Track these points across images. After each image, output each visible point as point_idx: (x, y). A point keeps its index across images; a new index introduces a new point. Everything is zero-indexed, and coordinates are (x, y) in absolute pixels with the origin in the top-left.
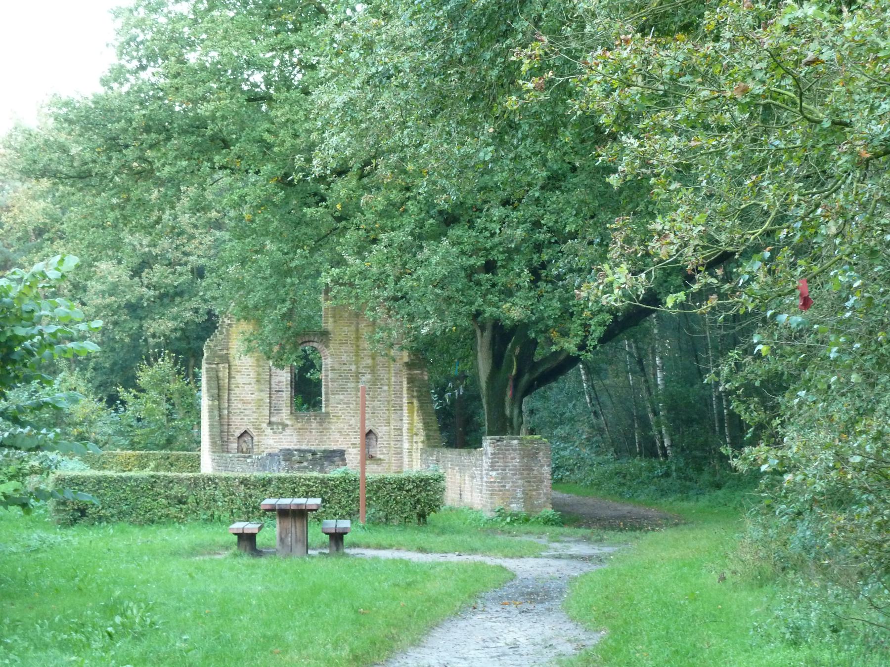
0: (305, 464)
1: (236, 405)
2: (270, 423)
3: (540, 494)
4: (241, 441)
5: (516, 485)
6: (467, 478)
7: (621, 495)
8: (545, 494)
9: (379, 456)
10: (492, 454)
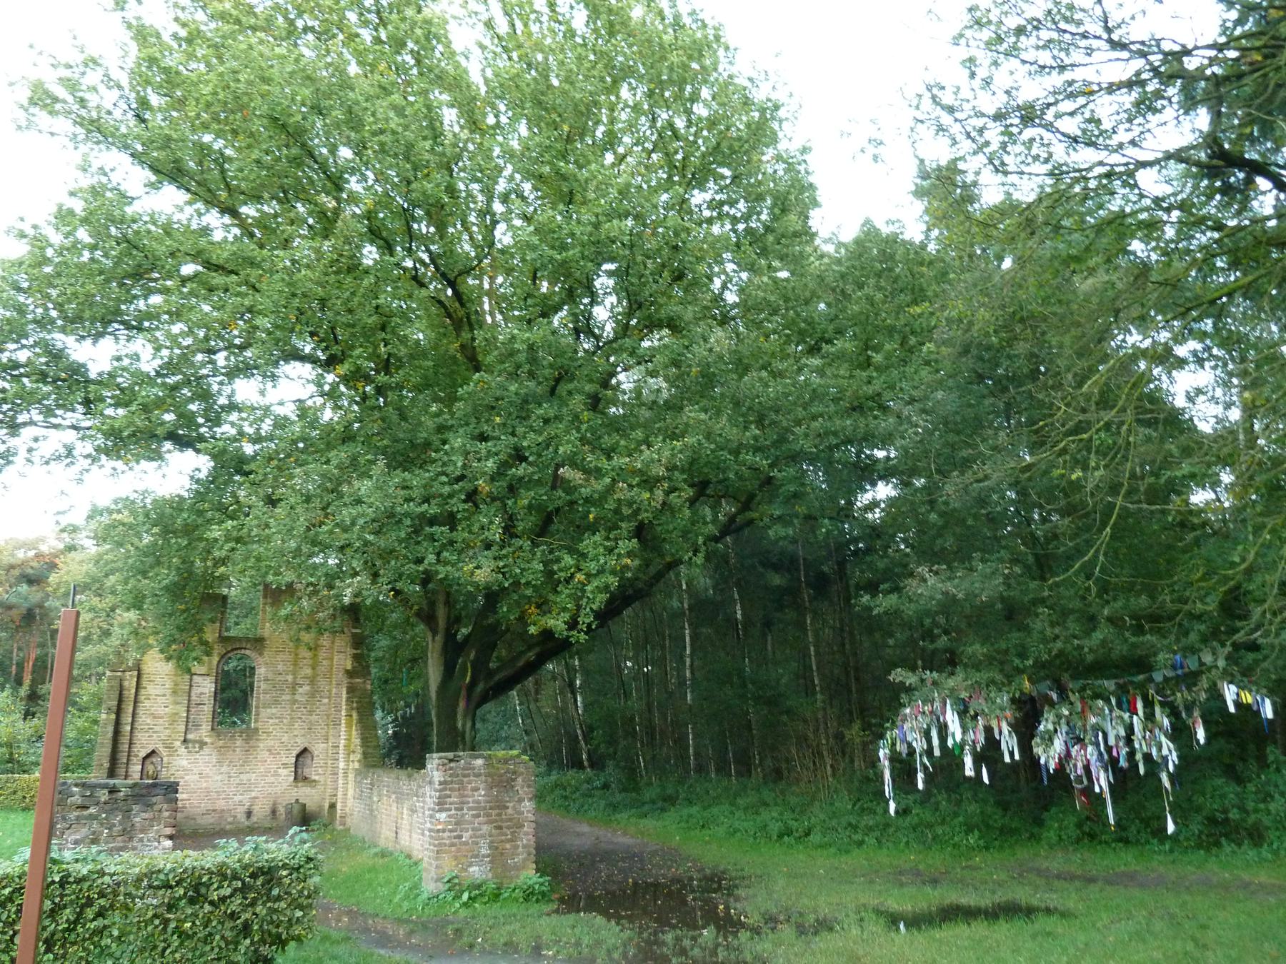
0: (93, 810)
1: (144, 719)
2: (185, 741)
3: (517, 847)
4: (148, 762)
5: (479, 833)
6: (405, 811)
7: (567, 808)
8: (524, 847)
9: (314, 777)
10: (441, 783)
